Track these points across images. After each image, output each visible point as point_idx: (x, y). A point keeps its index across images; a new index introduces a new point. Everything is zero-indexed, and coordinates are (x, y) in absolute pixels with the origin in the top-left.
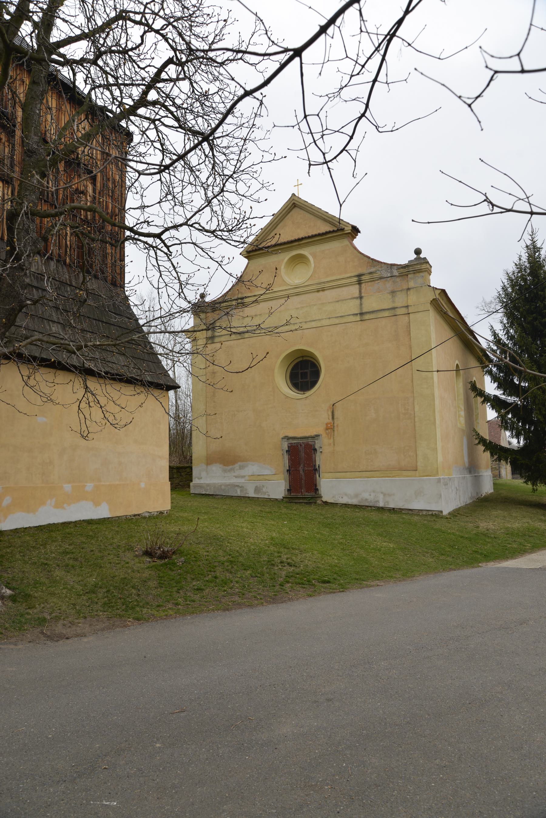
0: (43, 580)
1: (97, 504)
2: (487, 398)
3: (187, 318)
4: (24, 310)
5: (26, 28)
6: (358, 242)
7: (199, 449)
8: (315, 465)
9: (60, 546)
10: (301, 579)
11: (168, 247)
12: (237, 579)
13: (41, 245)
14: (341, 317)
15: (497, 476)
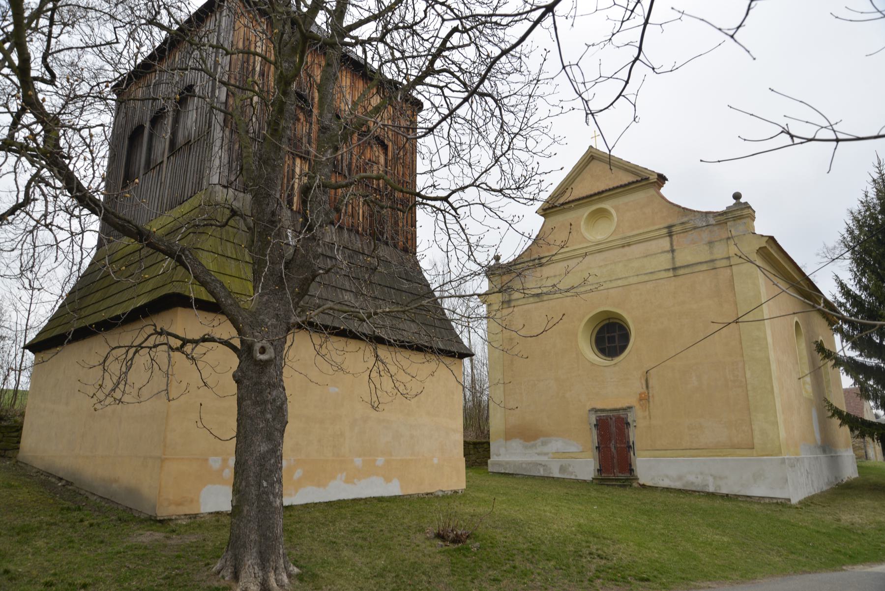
0: (331, 559)
1: (388, 480)
2: (839, 362)
3: (479, 281)
4: (318, 279)
5: (321, 18)
6: (665, 191)
7: (496, 423)
8: (628, 442)
9: (349, 524)
10: (615, 575)
11: (455, 210)
12: (538, 571)
13: (334, 216)
15: (862, 456)
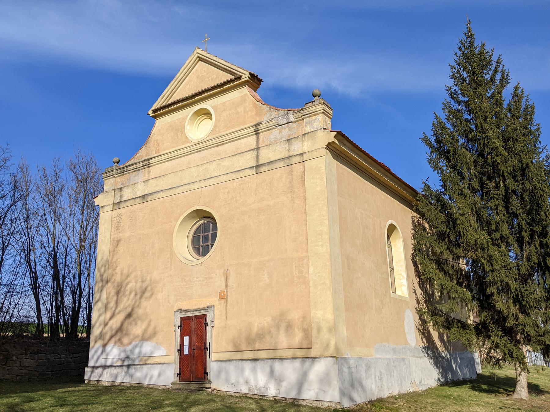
8: (205, 344)
14: (238, 171)
